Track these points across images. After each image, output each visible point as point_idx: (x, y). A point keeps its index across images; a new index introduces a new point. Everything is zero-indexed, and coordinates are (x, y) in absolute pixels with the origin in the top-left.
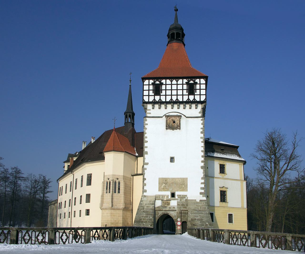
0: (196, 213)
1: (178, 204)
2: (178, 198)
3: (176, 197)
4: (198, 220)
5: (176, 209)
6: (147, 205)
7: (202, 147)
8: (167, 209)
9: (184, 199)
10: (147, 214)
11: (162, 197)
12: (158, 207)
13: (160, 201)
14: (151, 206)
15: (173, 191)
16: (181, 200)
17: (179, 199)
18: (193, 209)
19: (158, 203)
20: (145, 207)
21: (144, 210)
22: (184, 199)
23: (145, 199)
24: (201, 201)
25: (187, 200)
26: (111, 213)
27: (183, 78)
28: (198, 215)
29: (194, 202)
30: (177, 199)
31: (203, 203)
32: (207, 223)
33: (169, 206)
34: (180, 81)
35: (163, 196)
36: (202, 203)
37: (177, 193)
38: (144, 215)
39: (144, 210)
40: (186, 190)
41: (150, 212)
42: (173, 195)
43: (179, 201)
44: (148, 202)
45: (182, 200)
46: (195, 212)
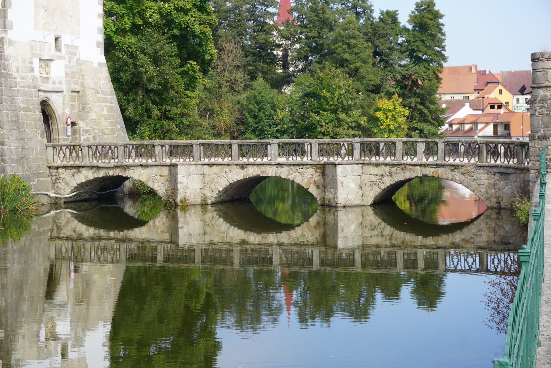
5: (64, 87)
15: (58, 34)
22: (75, 58)
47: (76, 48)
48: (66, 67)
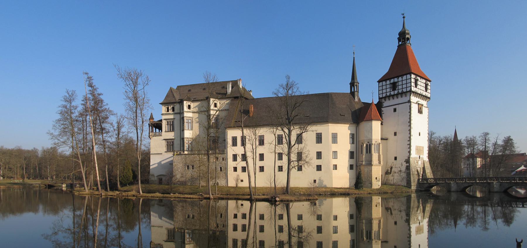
37: (421, 156)
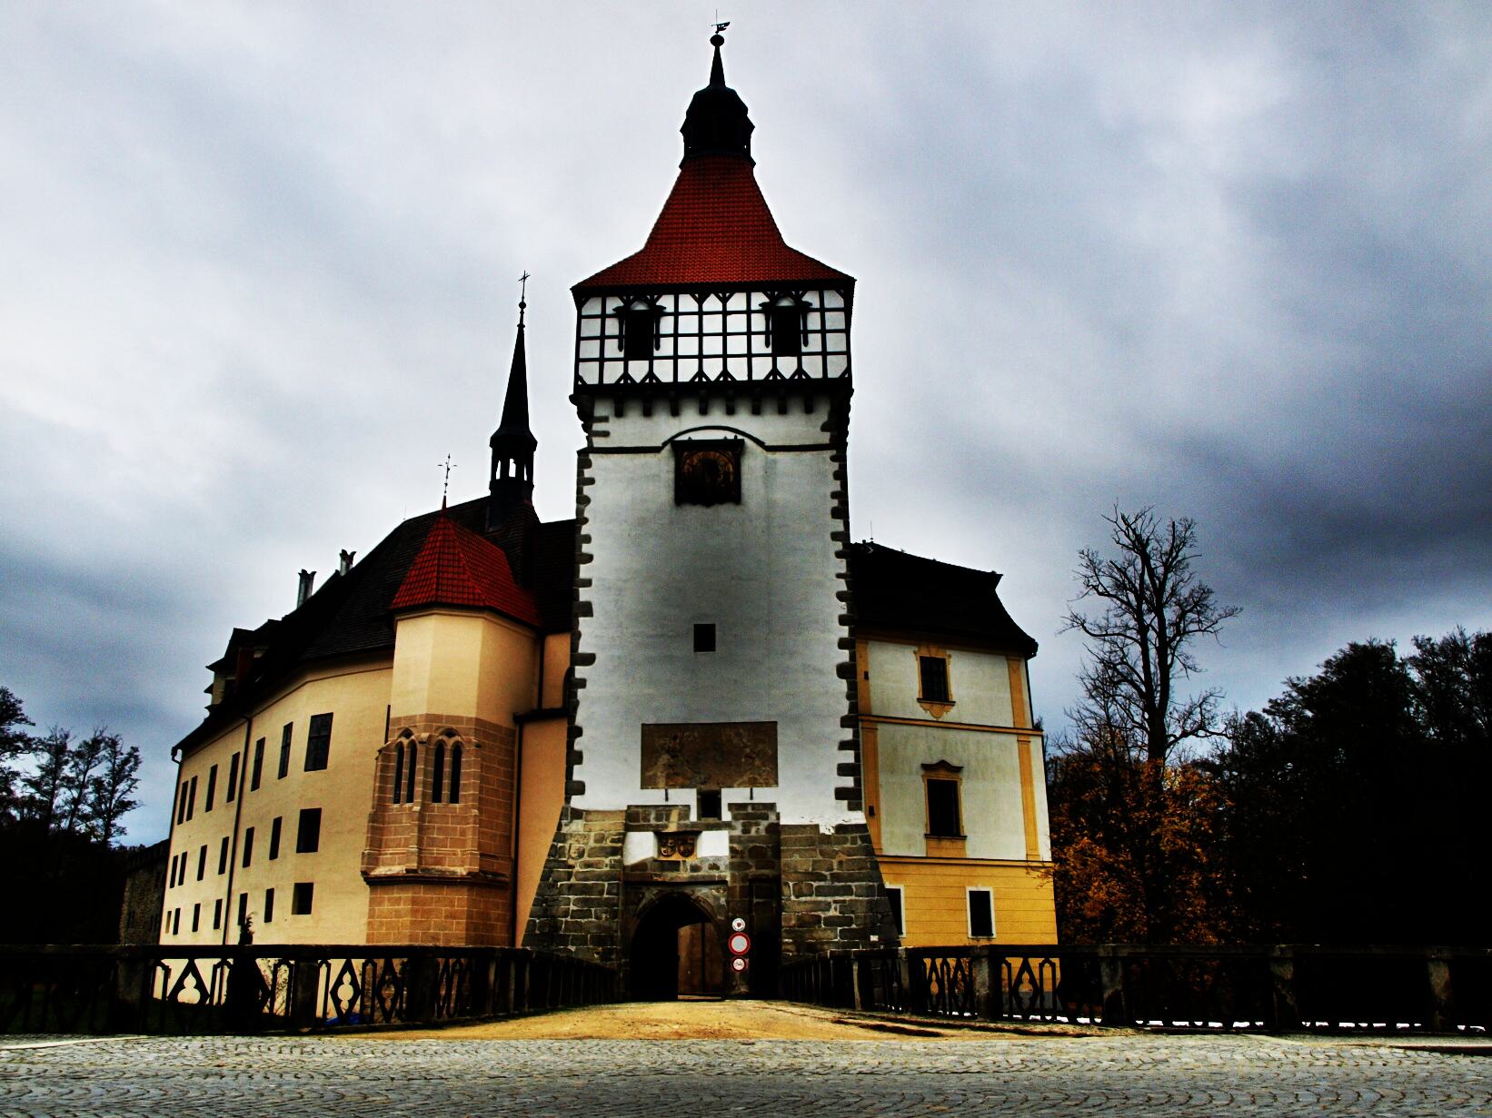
0: (820, 892)
1: (732, 850)
2: (735, 818)
3: (726, 816)
4: (831, 922)
6: (586, 858)
7: (839, 576)
8: (684, 874)
9: (764, 824)
10: (585, 902)
11: (658, 818)
12: (641, 866)
13: (651, 834)
14: (607, 861)
16: (746, 830)
17: (739, 825)
18: (806, 873)
19: (642, 847)
20: (577, 869)
21: (573, 881)
22: (764, 824)
23: (577, 826)
24: (840, 829)
25: (775, 829)
26: (414, 901)
27: (748, 289)
28: (829, 899)
29: (810, 834)
30: (728, 825)
31: (854, 841)
32: (874, 938)
33: (690, 861)
34: (738, 301)
35: (664, 811)
36: (845, 841)
38: (572, 907)
39: (573, 881)
40: (772, 779)
41: (601, 893)
42: (709, 805)
43: (738, 832)
44: (592, 843)
45: (753, 830)
46: (815, 884)
47: (772, 806)
48: (732, 839)
